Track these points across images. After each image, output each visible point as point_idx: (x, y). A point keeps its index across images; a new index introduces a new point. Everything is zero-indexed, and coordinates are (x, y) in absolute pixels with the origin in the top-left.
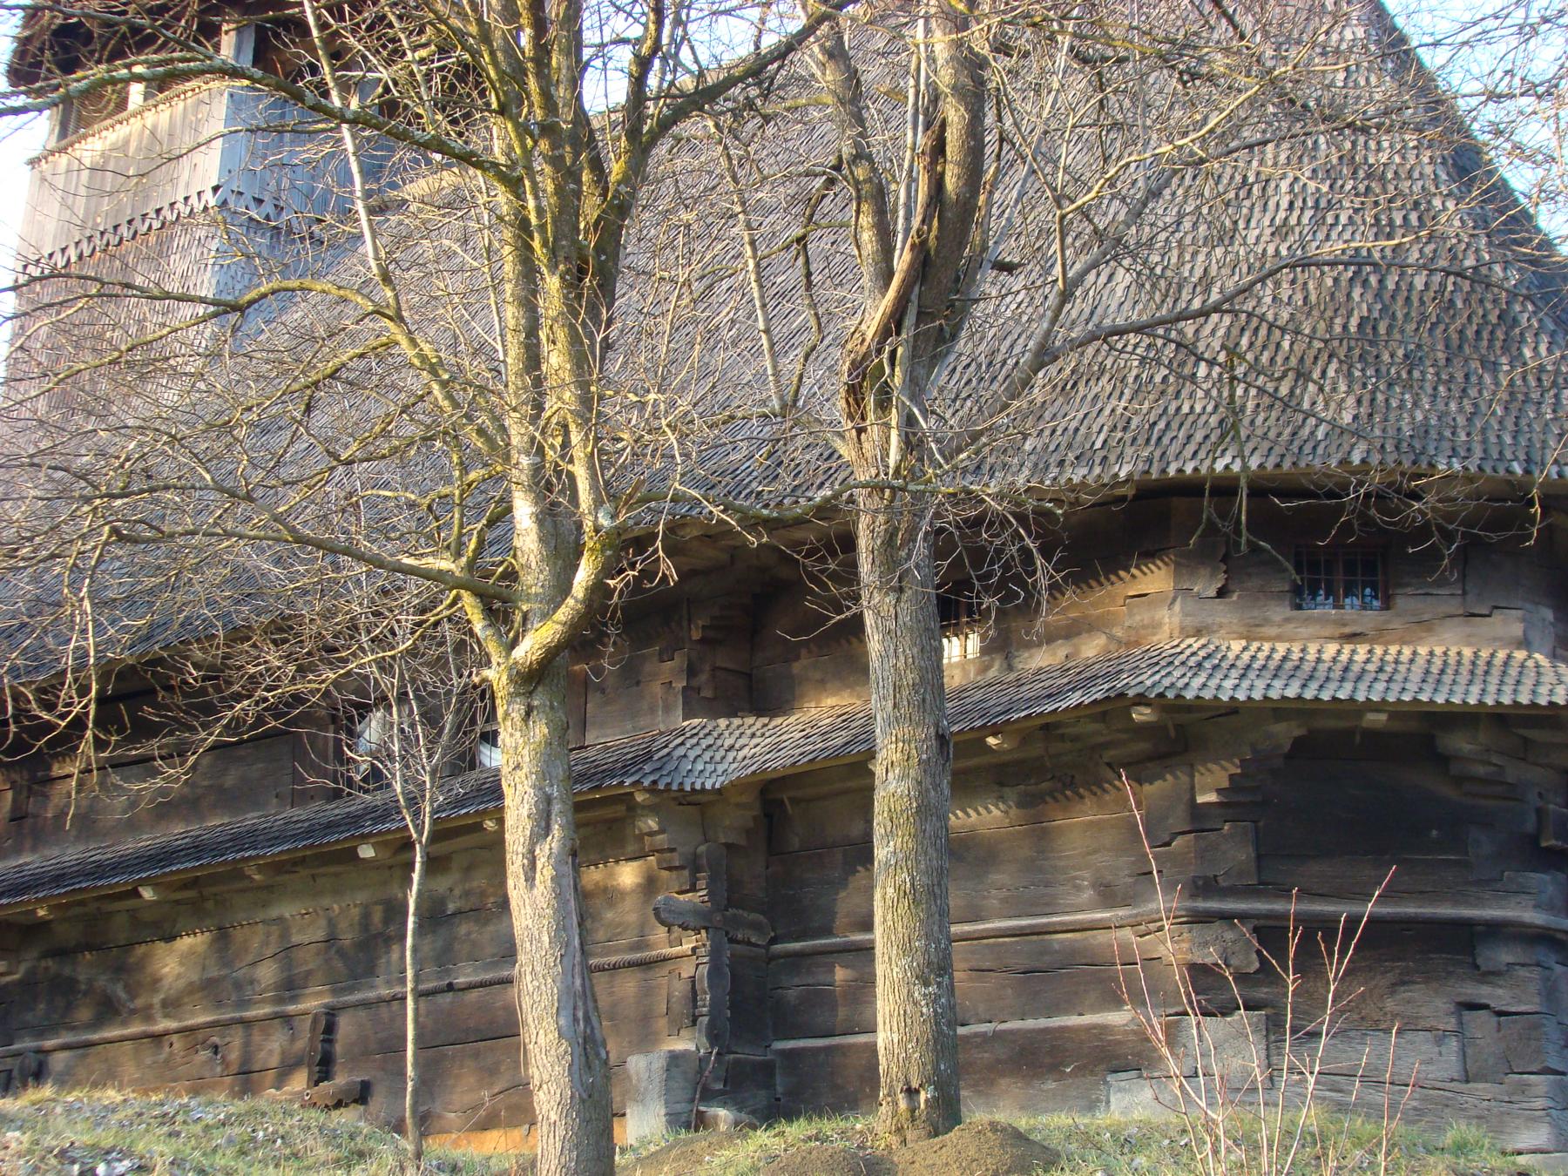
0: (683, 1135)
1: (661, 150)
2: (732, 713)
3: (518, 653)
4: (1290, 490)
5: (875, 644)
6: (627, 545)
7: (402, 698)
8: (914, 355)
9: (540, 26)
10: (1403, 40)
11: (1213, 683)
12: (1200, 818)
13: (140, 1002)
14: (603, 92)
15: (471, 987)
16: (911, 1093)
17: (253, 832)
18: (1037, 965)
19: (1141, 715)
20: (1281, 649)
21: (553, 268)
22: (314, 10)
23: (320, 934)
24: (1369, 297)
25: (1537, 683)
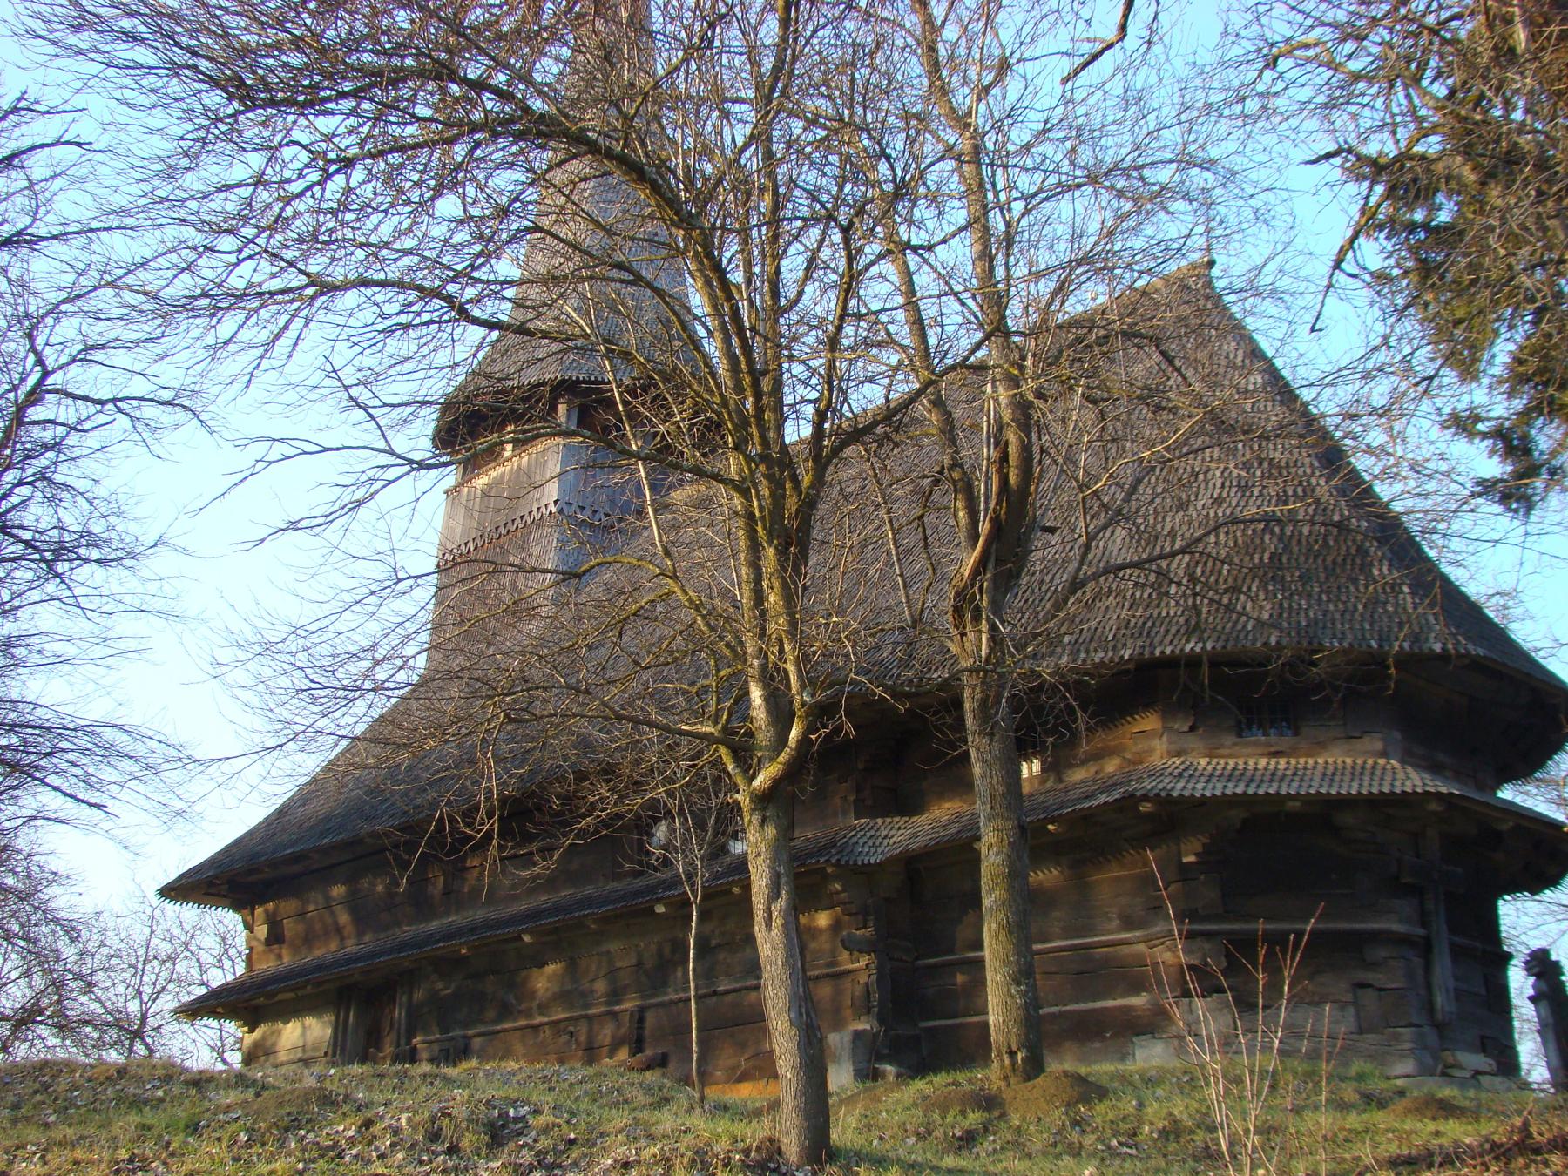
2: (885, 814)
3: (756, 783)
4: (1234, 664)
5: (977, 770)
6: (821, 712)
7: (681, 812)
9: (758, 396)
10: (1287, 384)
11: (1190, 786)
12: (1185, 872)
13: (523, 1007)
14: (797, 431)
15: (727, 992)
16: (1012, 1054)
17: (589, 897)
19: (1145, 808)
20: (1231, 763)
21: (770, 543)
22: (621, 394)
23: (633, 961)
24: (1275, 540)
25: (1394, 779)
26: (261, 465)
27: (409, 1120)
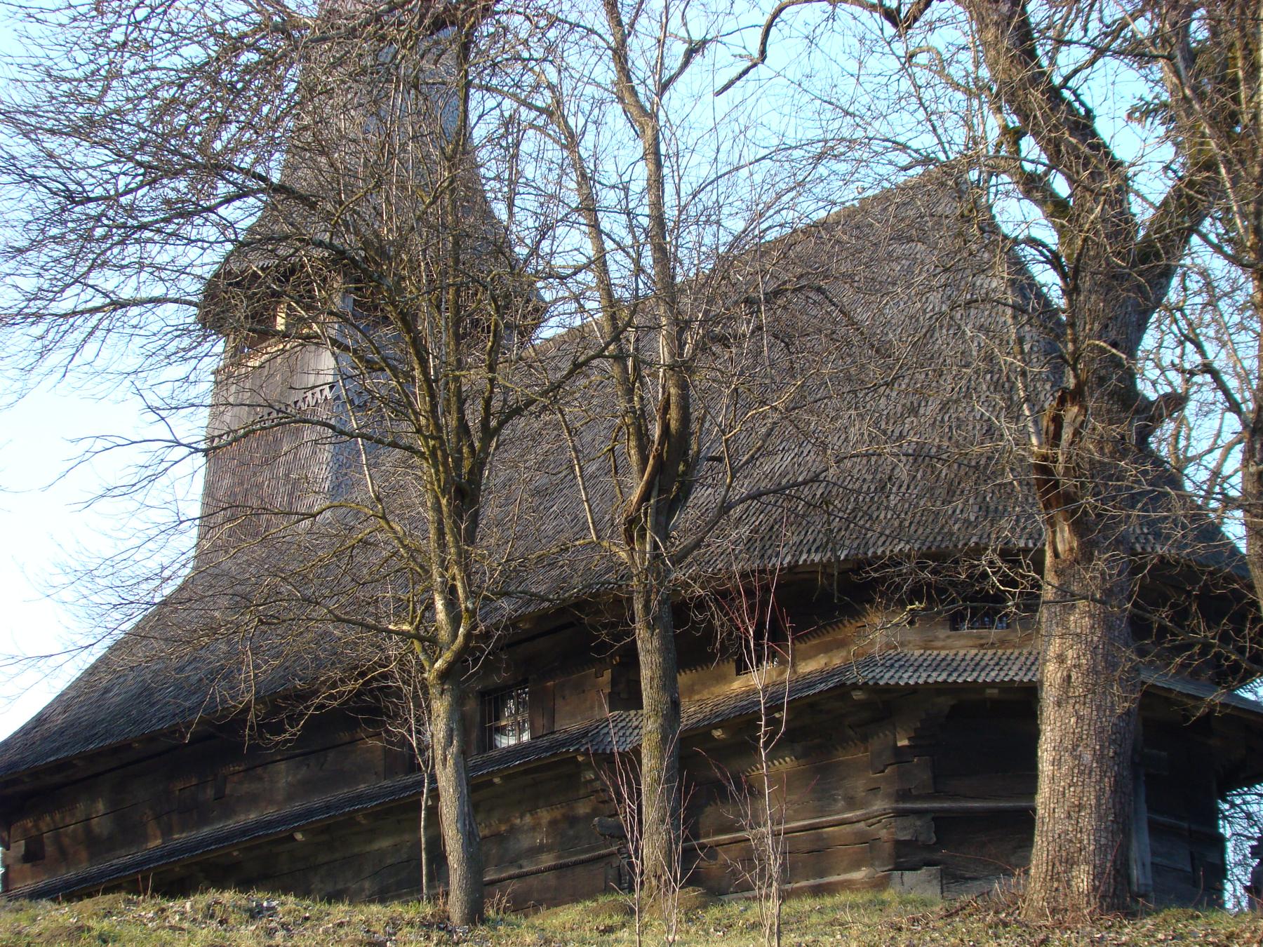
8: (658, 512)
11: (897, 676)
18: (816, 847)
19: (858, 695)
26: (88, 455)
27: (192, 907)
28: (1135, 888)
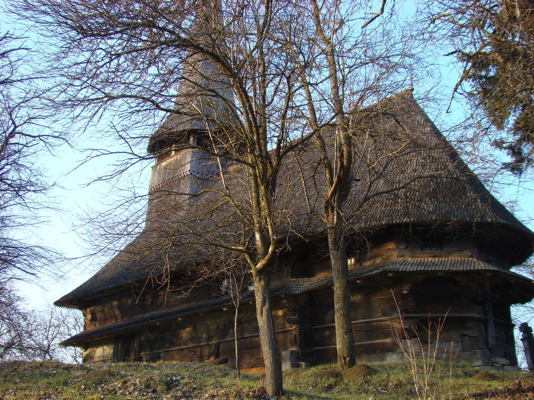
0: (296, 369)
1: (283, 159)
3: (258, 266)
5: (333, 262)
6: (279, 243)
7: (232, 276)
9: (258, 134)
10: (438, 131)
11: (405, 267)
12: (403, 297)
13: (178, 342)
14: (271, 147)
16: (345, 358)
19: (390, 275)
20: (419, 259)
22: (211, 134)
23: (216, 327)
24: (434, 184)
25: (475, 265)
26: (89, 158)
27: (139, 381)
28: (490, 346)
